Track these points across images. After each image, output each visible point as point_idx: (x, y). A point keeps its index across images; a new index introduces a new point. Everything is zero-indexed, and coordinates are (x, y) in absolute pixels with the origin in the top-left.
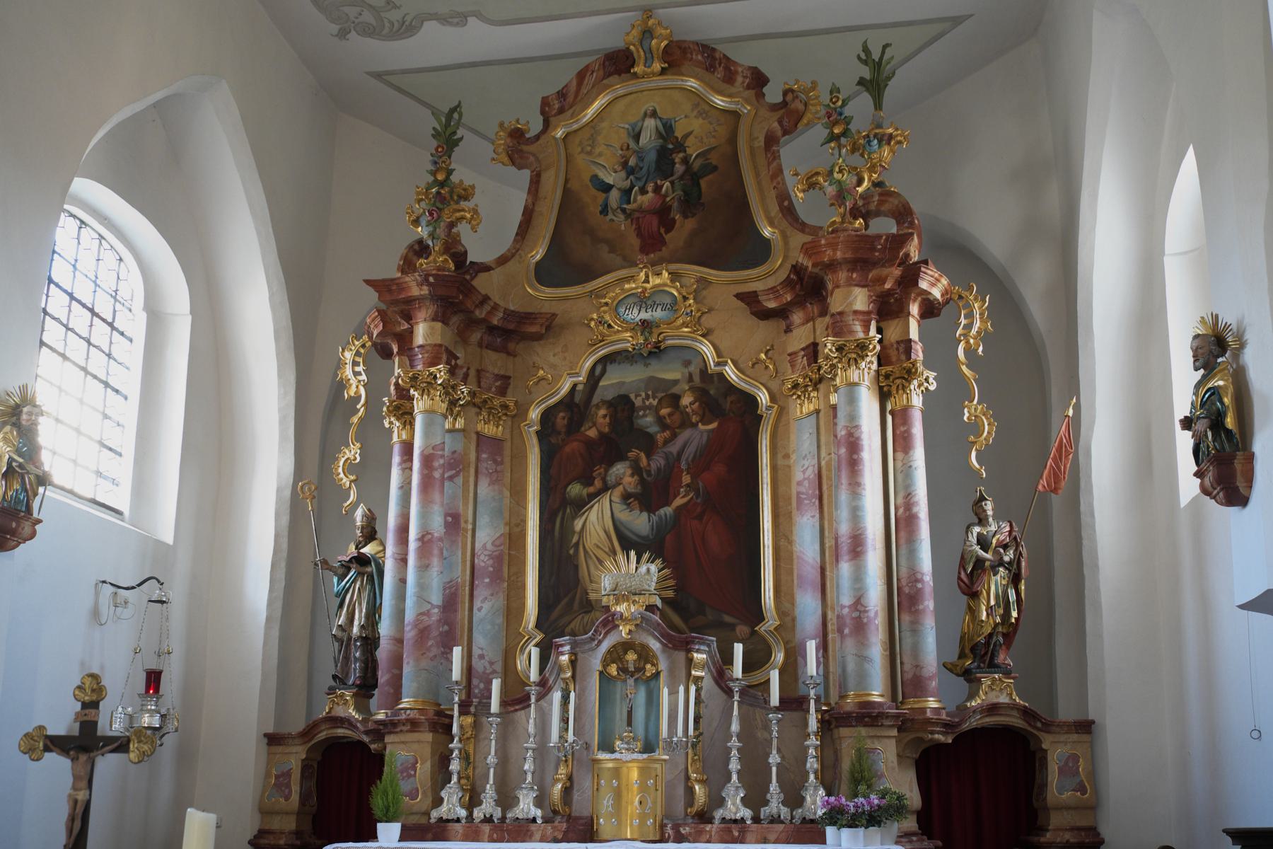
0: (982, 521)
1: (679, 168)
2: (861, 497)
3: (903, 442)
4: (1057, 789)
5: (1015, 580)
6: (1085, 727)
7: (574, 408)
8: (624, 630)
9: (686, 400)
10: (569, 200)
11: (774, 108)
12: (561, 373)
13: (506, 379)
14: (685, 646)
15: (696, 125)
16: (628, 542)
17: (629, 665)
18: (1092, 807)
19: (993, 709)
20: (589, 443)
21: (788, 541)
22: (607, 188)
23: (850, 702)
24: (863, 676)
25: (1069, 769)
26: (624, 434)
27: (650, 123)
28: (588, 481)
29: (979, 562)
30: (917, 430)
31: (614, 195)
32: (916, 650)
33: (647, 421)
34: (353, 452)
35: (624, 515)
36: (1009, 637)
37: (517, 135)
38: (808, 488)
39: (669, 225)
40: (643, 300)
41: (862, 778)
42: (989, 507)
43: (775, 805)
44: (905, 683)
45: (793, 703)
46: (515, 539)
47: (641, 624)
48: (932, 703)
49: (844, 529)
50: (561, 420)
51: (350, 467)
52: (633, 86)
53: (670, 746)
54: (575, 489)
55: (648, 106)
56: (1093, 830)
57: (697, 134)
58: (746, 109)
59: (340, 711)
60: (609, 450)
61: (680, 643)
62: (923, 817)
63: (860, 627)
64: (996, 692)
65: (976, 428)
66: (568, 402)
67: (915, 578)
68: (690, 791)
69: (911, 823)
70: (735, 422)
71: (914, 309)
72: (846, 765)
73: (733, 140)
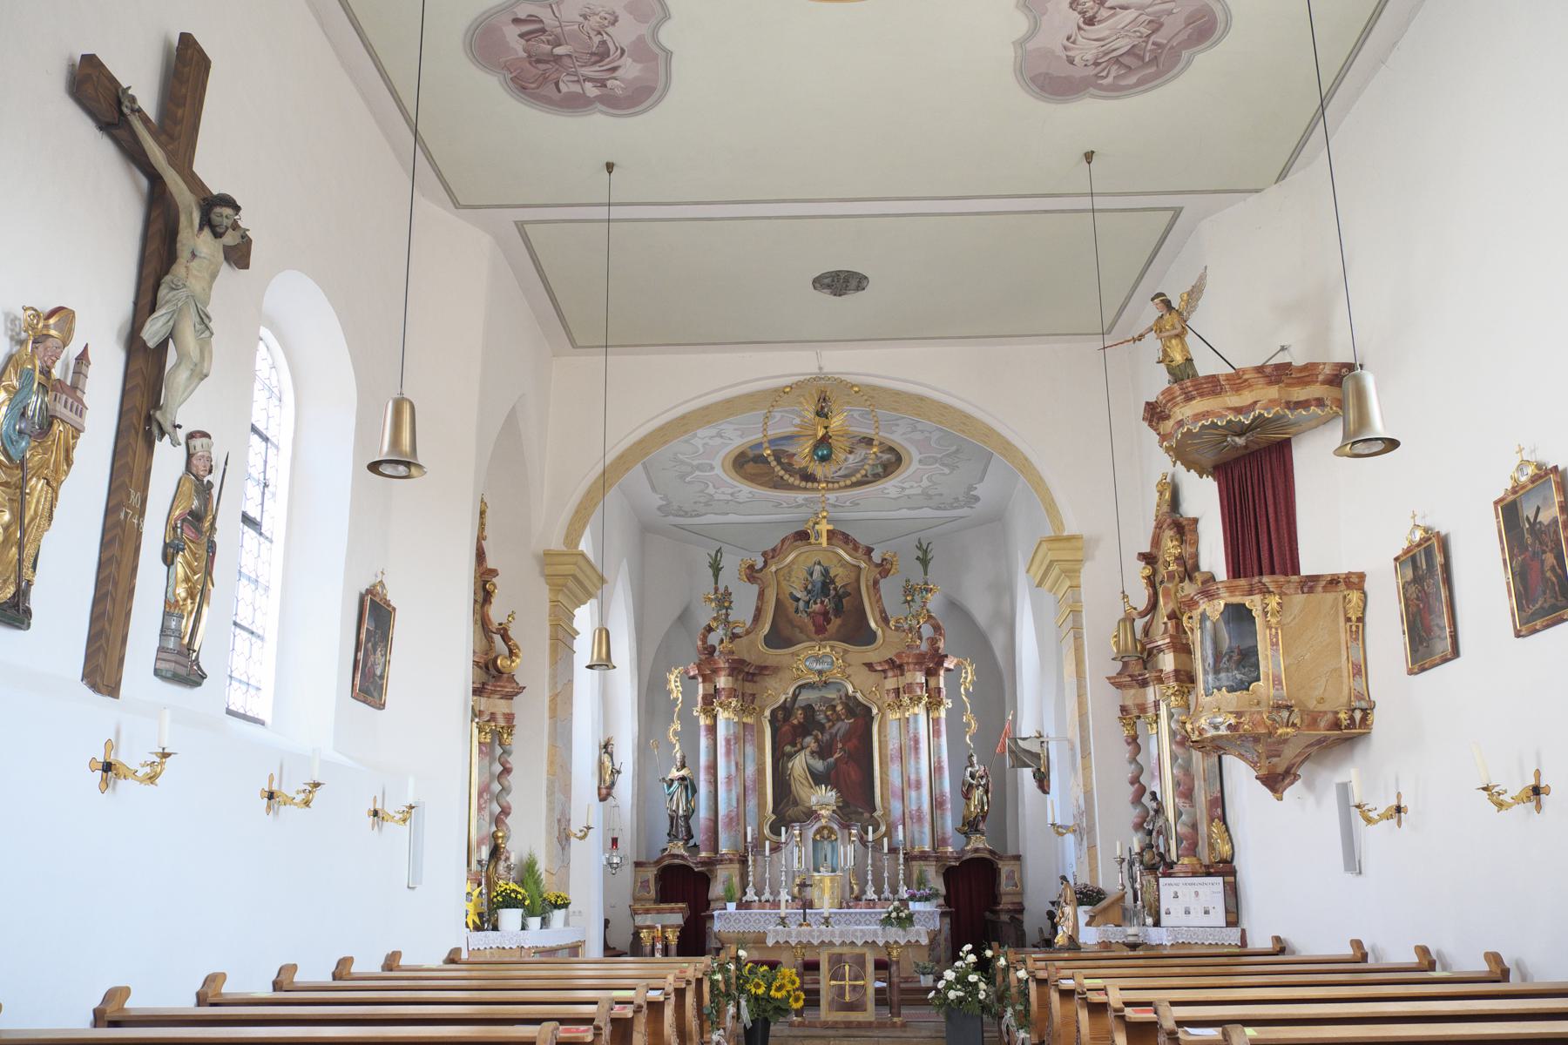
0: (972, 765)
1: (832, 593)
2: (918, 754)
3: (937, 733)
4: (1005, 886)
5: (987, 792)
6: (1018, 858)
7: (786, 710)
8: (823, 821)
9: (839, 708)
10: (779, 604)
11: (877, 565)
12: (778, 692)
13: (754, 695)
14: (848, 827)
15: (840, 571)
16: (818, 779)
17: (824, 834)
18: (1021, 894)
19: (976, 850)
20: (794, 727)
21: (886, 775)
22: (798, 600)
23: (916, 851)
24: (921, 840)
25: (1010, 876)
26: (810, 723)
27: (818, 568)
28: (794, 745)
29: (971, 785)
30: (943, 728)
31: (801, 604)
32: (943, 828)
33: (821, 717)
34: (677, 726)
35: (811, 761)
36: (984, 817)
37: (751, 567)
38: (896, 753)
39: (829, 622)
40: (818, 659)
41: (922, 882)
42: (975, 759)
43: (887, 894)
44: (938, 841)
45: (893, 850)
46: (761, 771)
47: (830, 819)
48: (950, 849)
49: (913, 777)
50: (780, 715)
51: (676, 733)
52: (806, 548)
53: (843, 870)
54: (788, 748)
55: (816, 559)
56: (1021, 904)
57: (841, 577)
58: (863, 565)
59: (676, 851)
60: (804, 730)
61: (846, 826)
62: (947, 898)
63: (920, 819)
64: (979, 842)
65: (968, 725)
66: (783, 707)
67: (942, 795)
68: (852, 889)
69: (941, 901)
70: (861, 716)
71: (942, 672)
72: (915, 877)
73: (858, 580)
